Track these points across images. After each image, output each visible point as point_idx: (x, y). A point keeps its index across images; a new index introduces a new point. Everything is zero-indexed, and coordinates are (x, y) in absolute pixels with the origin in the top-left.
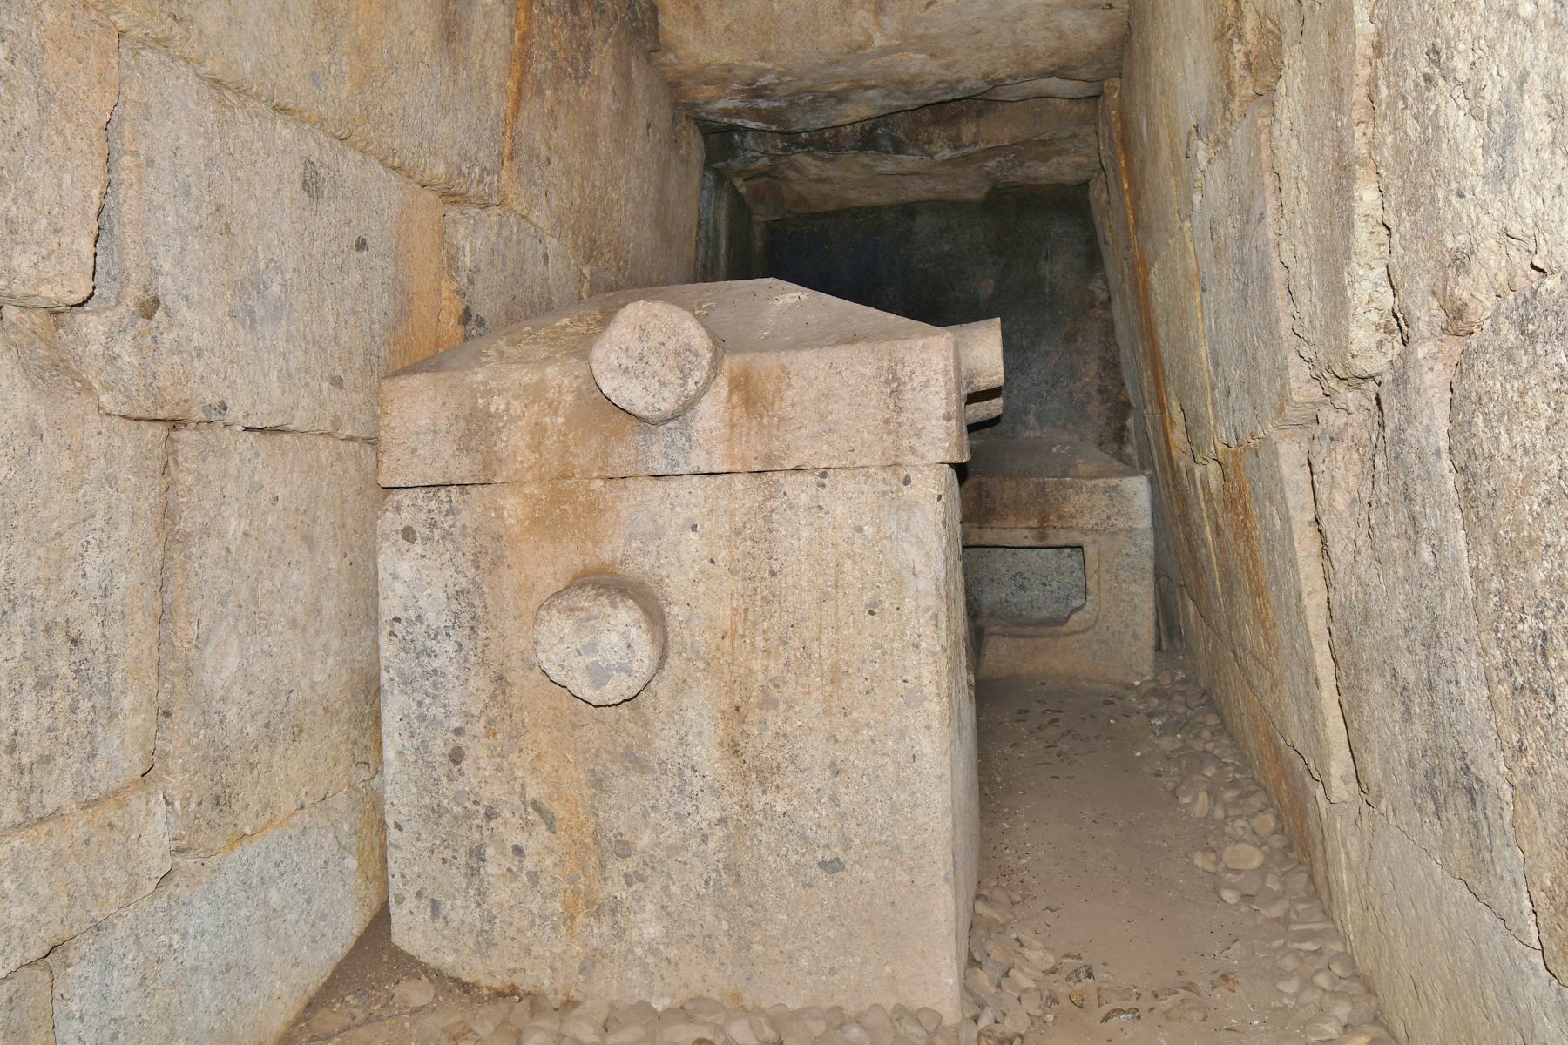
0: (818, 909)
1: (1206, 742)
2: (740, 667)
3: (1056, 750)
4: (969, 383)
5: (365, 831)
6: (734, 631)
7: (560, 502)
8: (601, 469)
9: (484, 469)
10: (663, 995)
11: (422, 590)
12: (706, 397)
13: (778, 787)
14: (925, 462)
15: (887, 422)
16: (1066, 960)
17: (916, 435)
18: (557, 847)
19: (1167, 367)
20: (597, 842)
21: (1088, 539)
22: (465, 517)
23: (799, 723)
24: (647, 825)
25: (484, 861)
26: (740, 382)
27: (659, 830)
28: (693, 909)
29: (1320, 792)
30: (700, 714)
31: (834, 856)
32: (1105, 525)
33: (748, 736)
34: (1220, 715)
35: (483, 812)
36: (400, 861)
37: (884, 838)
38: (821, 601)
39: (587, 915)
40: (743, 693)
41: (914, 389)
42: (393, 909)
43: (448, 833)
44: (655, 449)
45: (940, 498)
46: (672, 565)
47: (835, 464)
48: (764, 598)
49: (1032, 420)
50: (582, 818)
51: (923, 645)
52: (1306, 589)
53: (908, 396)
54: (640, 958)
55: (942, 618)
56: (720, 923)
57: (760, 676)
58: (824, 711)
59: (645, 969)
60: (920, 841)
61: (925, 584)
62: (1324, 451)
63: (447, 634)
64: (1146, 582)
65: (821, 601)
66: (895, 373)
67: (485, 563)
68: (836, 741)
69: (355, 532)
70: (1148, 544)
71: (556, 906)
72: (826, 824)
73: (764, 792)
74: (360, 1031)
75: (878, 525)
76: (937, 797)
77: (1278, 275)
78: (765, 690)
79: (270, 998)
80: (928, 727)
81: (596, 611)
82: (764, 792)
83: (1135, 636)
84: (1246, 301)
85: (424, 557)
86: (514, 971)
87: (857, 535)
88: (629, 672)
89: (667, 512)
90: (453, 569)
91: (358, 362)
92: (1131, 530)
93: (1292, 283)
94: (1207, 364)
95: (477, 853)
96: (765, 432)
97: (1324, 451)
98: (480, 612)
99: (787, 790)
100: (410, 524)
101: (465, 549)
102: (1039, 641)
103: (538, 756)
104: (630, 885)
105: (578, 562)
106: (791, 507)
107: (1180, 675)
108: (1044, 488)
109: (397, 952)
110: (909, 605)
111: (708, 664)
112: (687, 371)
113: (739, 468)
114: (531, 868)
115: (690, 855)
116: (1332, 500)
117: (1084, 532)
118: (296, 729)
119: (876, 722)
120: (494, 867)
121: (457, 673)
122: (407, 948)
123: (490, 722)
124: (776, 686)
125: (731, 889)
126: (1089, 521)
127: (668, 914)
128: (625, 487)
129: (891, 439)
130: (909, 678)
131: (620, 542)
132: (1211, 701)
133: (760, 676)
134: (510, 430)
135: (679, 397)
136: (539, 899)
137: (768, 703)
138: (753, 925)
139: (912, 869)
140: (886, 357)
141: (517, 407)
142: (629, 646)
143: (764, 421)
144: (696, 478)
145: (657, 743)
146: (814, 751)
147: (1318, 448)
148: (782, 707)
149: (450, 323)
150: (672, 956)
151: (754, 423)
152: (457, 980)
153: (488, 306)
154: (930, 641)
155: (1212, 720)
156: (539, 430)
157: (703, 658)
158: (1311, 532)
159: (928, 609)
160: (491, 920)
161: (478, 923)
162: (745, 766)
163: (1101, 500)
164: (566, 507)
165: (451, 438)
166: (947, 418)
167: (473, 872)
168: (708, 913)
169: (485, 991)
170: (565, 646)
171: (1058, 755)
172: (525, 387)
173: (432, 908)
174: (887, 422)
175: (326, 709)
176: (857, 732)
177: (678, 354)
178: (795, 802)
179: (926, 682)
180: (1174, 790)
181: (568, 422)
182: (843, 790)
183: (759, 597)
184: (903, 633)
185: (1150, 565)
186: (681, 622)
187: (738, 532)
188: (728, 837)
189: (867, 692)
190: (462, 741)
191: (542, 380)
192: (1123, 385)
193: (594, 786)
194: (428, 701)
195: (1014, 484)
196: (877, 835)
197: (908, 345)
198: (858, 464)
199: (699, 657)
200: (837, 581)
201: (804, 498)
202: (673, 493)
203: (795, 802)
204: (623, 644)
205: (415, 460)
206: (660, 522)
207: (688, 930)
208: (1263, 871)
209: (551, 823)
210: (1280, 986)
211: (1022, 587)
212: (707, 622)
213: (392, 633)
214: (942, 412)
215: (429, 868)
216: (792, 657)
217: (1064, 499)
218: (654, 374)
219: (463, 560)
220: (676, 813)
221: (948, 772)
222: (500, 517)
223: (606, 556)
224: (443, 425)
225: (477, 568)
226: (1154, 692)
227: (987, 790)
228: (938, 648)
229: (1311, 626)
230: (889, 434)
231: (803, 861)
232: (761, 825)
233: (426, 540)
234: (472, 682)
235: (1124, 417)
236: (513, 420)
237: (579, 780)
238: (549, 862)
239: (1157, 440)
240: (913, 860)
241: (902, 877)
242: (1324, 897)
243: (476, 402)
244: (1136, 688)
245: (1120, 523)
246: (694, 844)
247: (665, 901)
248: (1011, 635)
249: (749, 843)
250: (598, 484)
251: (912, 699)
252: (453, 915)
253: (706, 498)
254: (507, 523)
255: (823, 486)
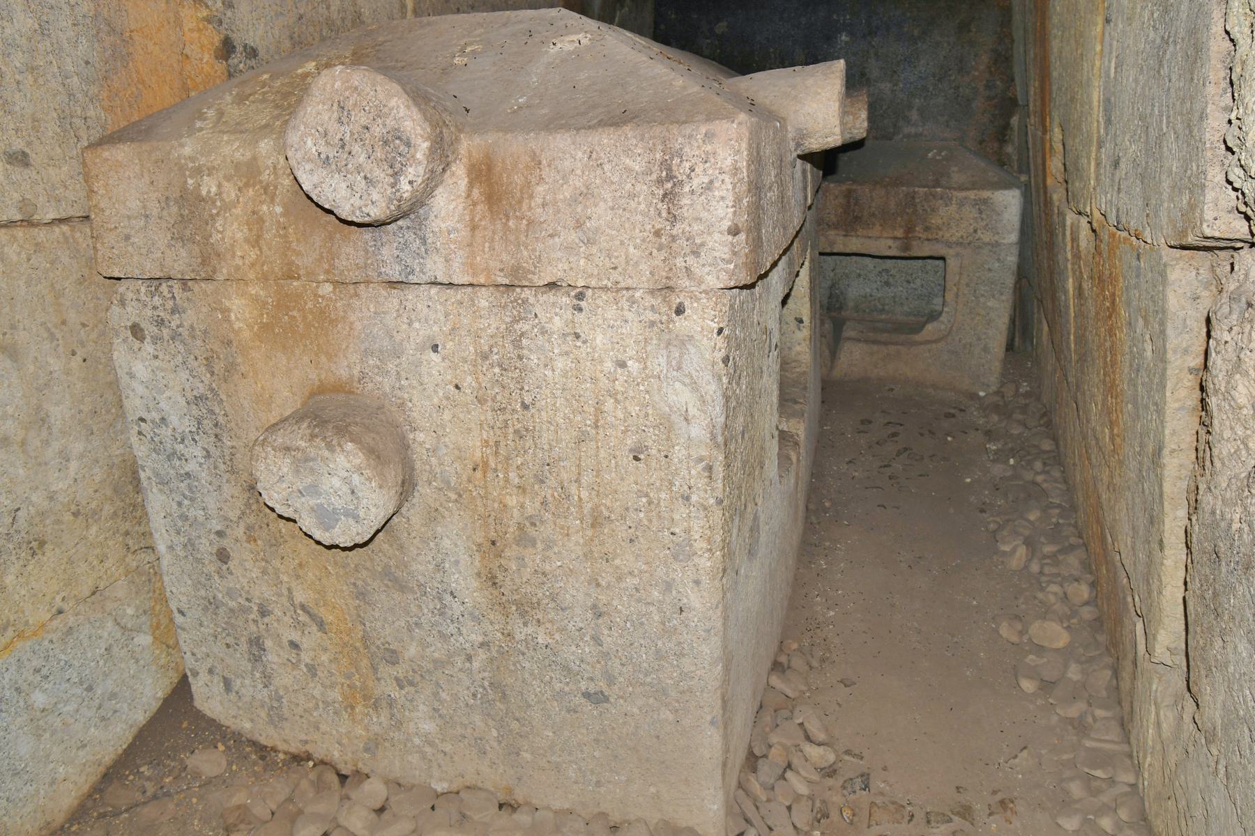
0: (584, 731)
1: (1038, 473)
2: (494, 501)
3: (888, 471)
4: (798, 145)
5: (158, 608)
6: (486, 464)
7: (288, 307)
8: (327, 272)
9: (203, 263)
10: (441, 780)
11: (162, 392)
12: (440, 190)
13: (538, 621)
14: (703, 287)
15: (657, 234)
16: (847, 758)
17: (693, 252)
18: (329, 647)
19: (1055, 88)
20: (366, 647)
21: (951, 252)
22: (190, 317)
23: (559, 564)
24: (412, 639)
25: (264, 650)
26: (480, 171)
27: (424, 645)
28: (464, 715)
29: (1139, 626)
30: (456, 545)
31: (598, 689)
32: (970, 238)
33: (506, 570)
34: (1055, 439)
35: (256, 608)
36: (188, 641)
37: (648, 680)
38: (580, 441)
39: (366, 706)
40: (498, 527)
41: (692, 192)
42: (191, 679)
43: (226, 623)
44: (385, 251)
45: (720, 331)
46: (414, 388)
47: (593, 283)
48: (516, 432)
49: (914, 115)
50: (350, 625)
51: (694, 498)
52: (1170, 444)
53: (685, 201)
54: (418, 746)
55: (719, 471)
56: (490, 730)
57: (516, 512)
58: (585, 555)
59: (424, 757)
60: (686, 687)
61: (698, 430)
62: (1235, 317)
63: (194, 439)
64: (1004, 298)
65: (580, 441)
66: (669, 169)
67: (219, 367)
68: (598, 585)
69: (84, 325)
70: (1012, 259)
71: (335, 695)
72: (589, 659)
73: (525, 624)
74: (146, 810)
75: (643, 360)
76: (706, 649)
77: (1218, 45)
78: (521, 527)
79: (53, 783)
80: (697, 582)
81: (312, 452)
82: (525, 624)
83: (986, 349)
84: (1161, 64)
85: (156, 357)
86: (306, 742)
87: (619, 370)
88: (356, 518)
89: (405, 327)
90: (187, 372)
91: (51, 128)
92: (997, 244)
93: (1238, 70)
94: (1097, 113)
95: (256, 643)
96: (512, 238)
97: (1235, 317)
98: (221, 419)
99: (549, 625)
100: (137, 320)
101: (197, 352)
102: (892, 348)
103: (300, 565)
104: (402, 688)
105: (313, 376)
106: (543, 332)
107: (1025, 388)
108: (913, 198)
109: (199, 715)
110: (679, 453)
111: (460, 496)
112: (398, 166)
113: (482, 281)
114: (308, 661)
115: (456, 670)
116: (1231, 388)
117: (949, 244)
118: (34, 544)
119: (641, 572)
120: (273, 657)
121: (209, 479)
122: (209, 713)
123: (249, 528)
124: (534, 524)
125: (498, 704)
126: (954, 234)
127: (440, 715)
128: (356, 295)
129: (663, 254)
130: (677, 531)
131: (355, 358)
132: (1049, 426)
133: (516, 512)
134: (226, 218)
135: (391, 200)
136: (319, 687)
137: (523, 539)
138: (521, 736)
139: (677, 711)
140: (660, 147)
141: (230, 192)
142: (353, 492)
143: (511, 223)
144: (434, 290)
145: (414, 567)
146: (575, 592)
147: (1226, 309)
148: (540, 546)
149: (204, 60)
150: (447, 750)
151: (499, 226)
152: (254, 743)
153: (260, 32)
154: (702, 494)
155: (1047, 445)
156: (255, 221)
157: (455, 489)
158: (1190, 381)
159: (701, 459)
160: (279, 699)
161: (267, 700)
162: (504, 598)
163: (970, 212)
164: (295, 313)
165: (164, 225)
166: (734, 231)
167: (256, 659)
168: (477, 719)
169: (281, 756)
170: (284, 485)
171: (890, 478)
172: (237, 166)
173: (225, 685)
174: (657, 234)
175: (76, 514)
176: (619, 579)
177: (386, 143)
178: (557, 636)
179: (697, 537)
180: (994, 532)
181: (286, 213)
182: (606, 632)
183: (511, 430)
184: (671, 484)
185: (1010, 281)
186: (428, 450)
187: (485, 357)
188: (492, 660)
189: (631, 541)
190: (225, 543)
191: (254, 158)
192: (1013, 80)
193: (357, 598)
194: (186, 502)
195: (883, 192)
196: (641, 676)
197: (688, 131)
198: (622, 285)
199: (449, 488)
200: (597, 421)
201: (558, 323)
202: (409, 306)
203: (557, 636)
204: (346, 489)
205: (130, 248)
206: (398, 338)
207: (459, 730)
208: (1067, 654)
209: (321, 625)
210: (1061, 821)
211: (887, 284)
212: (456, 452)
213: (140, 433)
214: (727, 224)
215: (216, 650)
216: (548, 496)
217: (933, 210)
218: (359, 169)
219: (196, 364)
220: (439, 631)
221: (719, 624)
222: (227, 319)
223: (343, 373)
224: (154, 207)
225: (212, 373)
226: (996, 408)
227: (813, 519)
228: (712, 501)
229: (1167, 487)
230: (659, 250)
231: (567, 689)
232: (523, 654)
233: (156, 339)
234: (225, 487)
235: (1010, 115)
236: (227, 207)
237: (342, 591)
238: (324, 658)
239: (1035, 157)
240: (678, 701)
241: (667, 715)
242: (1126, 705)
243: (186, 182)
244: (979, 398)
245: (987, 237)
246: (459, 661)
247: (436, 704)
248: (866, 341)
249: (512, 668)
250: (327, 289)
251: (682, 552)
252: (243, 691)
253: (446, 315)
254: (236, 327)
255: (580, 310)
